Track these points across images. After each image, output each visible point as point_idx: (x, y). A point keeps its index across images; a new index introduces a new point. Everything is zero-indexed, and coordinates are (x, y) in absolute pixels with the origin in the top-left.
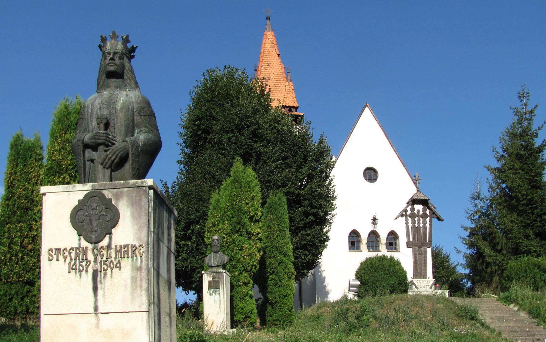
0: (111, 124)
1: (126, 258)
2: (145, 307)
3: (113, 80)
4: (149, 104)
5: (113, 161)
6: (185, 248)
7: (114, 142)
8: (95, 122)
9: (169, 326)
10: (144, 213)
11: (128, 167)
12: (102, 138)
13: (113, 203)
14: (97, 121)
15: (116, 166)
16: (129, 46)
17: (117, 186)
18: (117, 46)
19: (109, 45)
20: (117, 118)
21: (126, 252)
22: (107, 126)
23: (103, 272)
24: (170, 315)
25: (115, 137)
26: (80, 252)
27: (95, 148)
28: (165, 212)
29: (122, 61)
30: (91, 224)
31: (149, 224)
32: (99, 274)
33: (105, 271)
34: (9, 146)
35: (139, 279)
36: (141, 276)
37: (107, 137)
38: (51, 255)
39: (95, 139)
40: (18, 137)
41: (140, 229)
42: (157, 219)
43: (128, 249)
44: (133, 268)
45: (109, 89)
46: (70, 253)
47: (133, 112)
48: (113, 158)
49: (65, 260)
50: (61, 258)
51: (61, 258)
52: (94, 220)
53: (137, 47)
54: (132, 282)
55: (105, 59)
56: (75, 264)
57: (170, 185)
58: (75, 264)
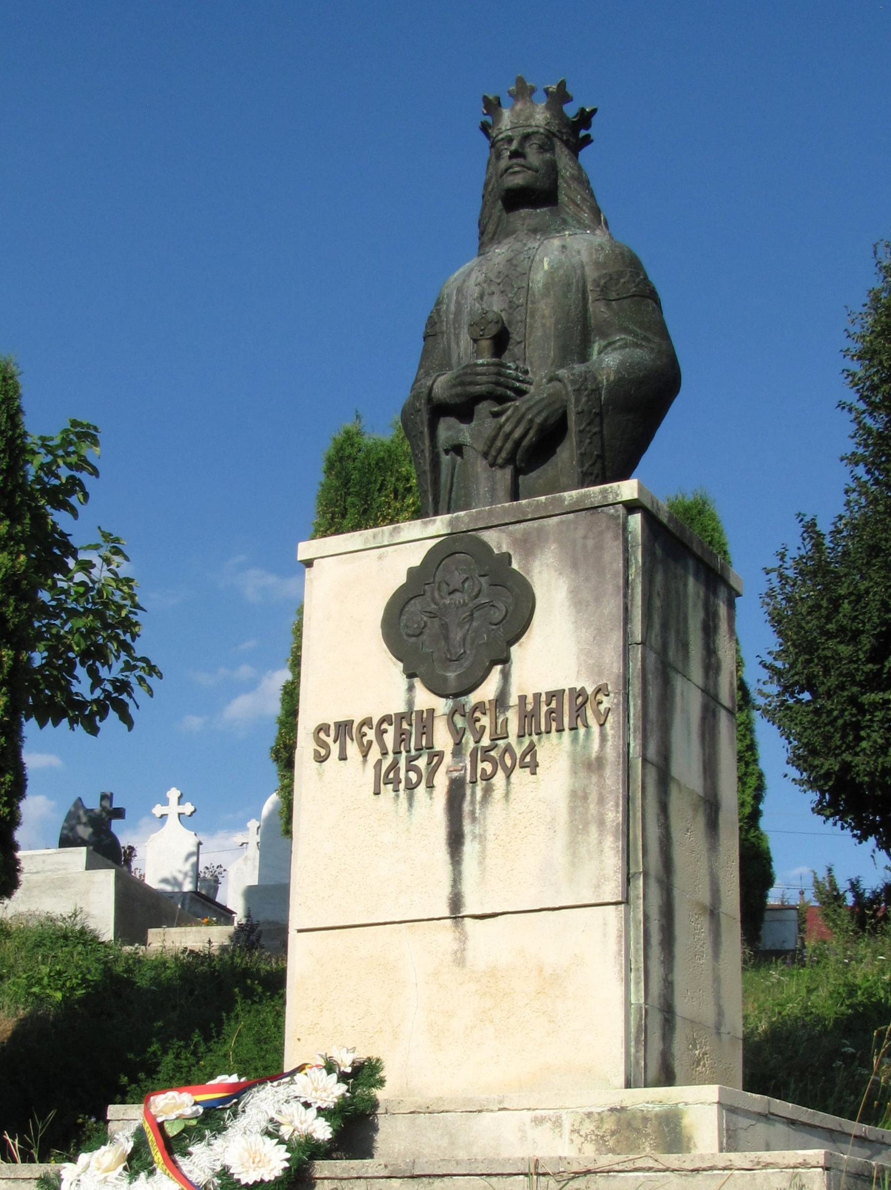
0: (515, 337)
1: (554, 734)
2: (612, 890)
3: (524, 212)
4: (634, 264)
5: (518, 443)
6: (879, 715)
7: (524, 386)
8: (465, 339)
9: (708, 949)
10: (610, 588)
11: (566, 454)
12: (484, 379)
13: (515, 566)
14: (470, 333)
15: (530, 456)
16: (571, 111)
17: (525, 513)
18: (531, 116)
19: (507, 118)
20: (533, 316)
21: (554, 715)
22: (501, 342)
23: (480, 785)
24: (713, 913)
25: (526, 372)
26: (411, 726)
27: (463, 410)
28: (691, 581)
29: (548, 156)
30: (447, 638)
31: (627, 619)
32: (468, 792)
33: (487, 778)
34: (323, 466)
35: (593, 797)
36: (601, 786)
37: (499, 374)
38: (324, 745)
39: (462, 384)
40: (349, 438)
41: (599, 636)
42: (657, 603)
43: (560, 704)
44: (574, 763)
45: (511, 239)
46: (381, 733)
47: (584, 292)
48: (517, 434)
49: (365, 756)
50: (353, 749)
51: (353, 749)
52: (454, 627)
53: (594, 111)
54: (572, 810)
55: (498, 156)
56: (394, 766)
57: (825, 527)
58: (394, 766)
